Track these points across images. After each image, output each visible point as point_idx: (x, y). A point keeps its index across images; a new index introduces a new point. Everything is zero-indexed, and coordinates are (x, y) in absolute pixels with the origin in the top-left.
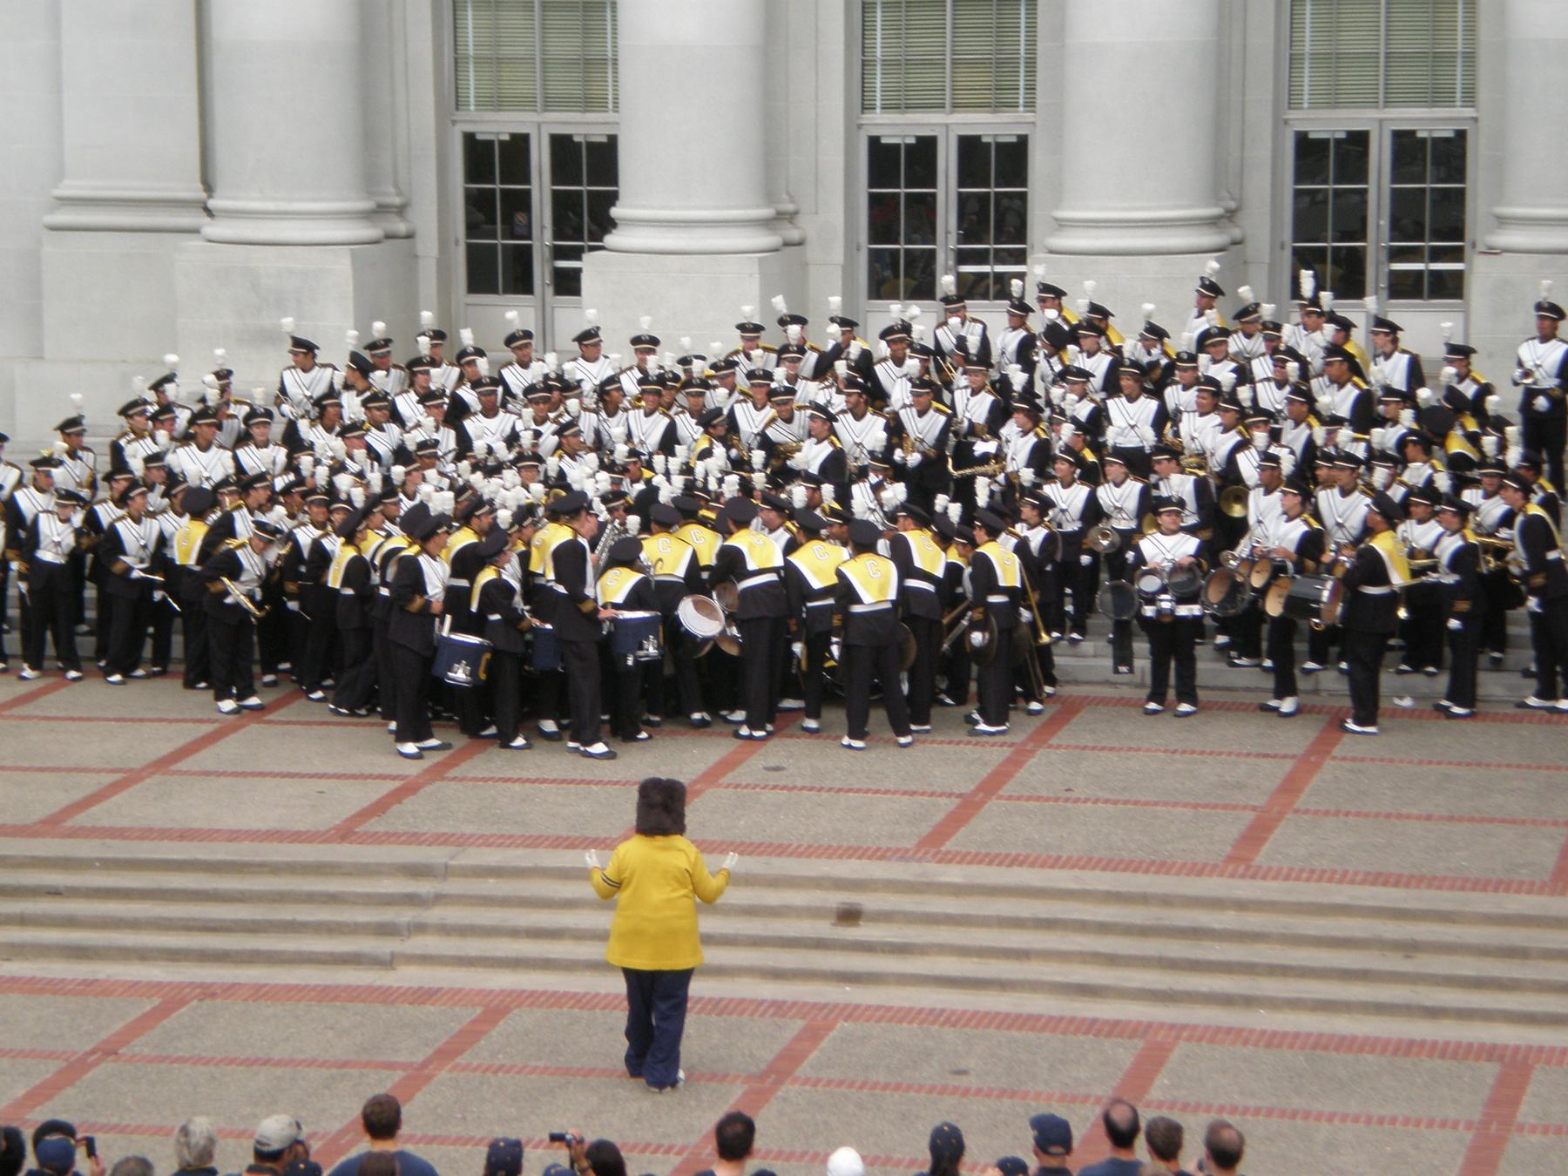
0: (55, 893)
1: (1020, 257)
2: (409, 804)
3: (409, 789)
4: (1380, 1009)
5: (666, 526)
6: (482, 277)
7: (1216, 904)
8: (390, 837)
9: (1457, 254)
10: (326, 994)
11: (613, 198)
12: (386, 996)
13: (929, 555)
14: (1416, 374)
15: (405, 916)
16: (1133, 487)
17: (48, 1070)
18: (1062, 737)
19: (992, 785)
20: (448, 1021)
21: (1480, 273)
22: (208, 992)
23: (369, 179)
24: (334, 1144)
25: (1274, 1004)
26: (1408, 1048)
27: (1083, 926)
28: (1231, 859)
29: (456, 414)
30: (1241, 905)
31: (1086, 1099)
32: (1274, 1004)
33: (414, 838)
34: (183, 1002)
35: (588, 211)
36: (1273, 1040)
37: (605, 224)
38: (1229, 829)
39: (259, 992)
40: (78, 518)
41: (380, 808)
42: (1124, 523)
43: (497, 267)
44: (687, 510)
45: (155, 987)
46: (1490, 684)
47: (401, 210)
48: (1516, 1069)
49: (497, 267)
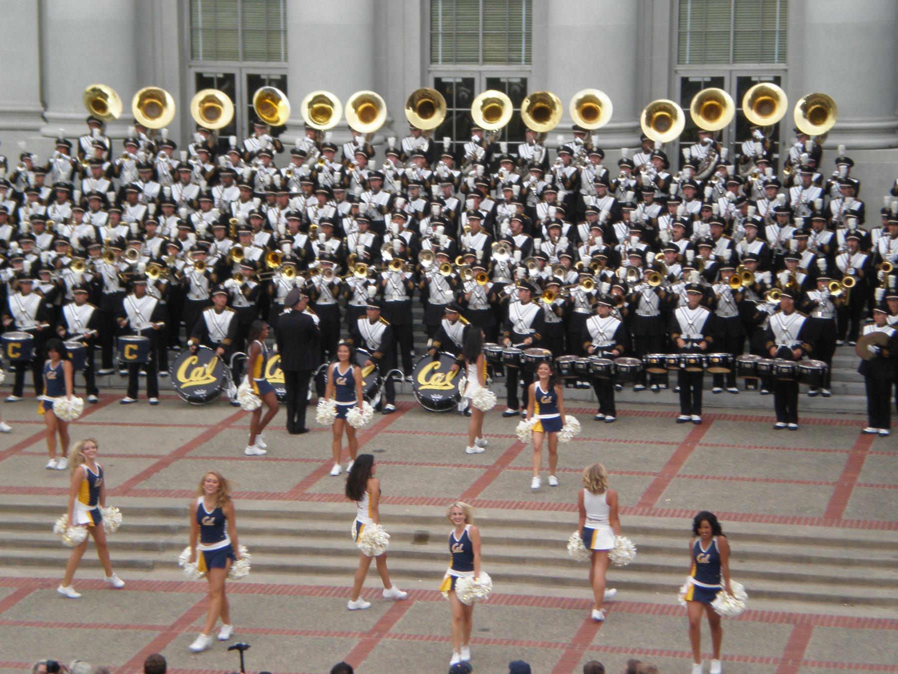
2: (164, 473)
8: (154, 493)
12: (150, 586)
28: (640, 504)
31: (556, 645)
33: (166, 493)
34: (31, 590)
48: (803, 628)
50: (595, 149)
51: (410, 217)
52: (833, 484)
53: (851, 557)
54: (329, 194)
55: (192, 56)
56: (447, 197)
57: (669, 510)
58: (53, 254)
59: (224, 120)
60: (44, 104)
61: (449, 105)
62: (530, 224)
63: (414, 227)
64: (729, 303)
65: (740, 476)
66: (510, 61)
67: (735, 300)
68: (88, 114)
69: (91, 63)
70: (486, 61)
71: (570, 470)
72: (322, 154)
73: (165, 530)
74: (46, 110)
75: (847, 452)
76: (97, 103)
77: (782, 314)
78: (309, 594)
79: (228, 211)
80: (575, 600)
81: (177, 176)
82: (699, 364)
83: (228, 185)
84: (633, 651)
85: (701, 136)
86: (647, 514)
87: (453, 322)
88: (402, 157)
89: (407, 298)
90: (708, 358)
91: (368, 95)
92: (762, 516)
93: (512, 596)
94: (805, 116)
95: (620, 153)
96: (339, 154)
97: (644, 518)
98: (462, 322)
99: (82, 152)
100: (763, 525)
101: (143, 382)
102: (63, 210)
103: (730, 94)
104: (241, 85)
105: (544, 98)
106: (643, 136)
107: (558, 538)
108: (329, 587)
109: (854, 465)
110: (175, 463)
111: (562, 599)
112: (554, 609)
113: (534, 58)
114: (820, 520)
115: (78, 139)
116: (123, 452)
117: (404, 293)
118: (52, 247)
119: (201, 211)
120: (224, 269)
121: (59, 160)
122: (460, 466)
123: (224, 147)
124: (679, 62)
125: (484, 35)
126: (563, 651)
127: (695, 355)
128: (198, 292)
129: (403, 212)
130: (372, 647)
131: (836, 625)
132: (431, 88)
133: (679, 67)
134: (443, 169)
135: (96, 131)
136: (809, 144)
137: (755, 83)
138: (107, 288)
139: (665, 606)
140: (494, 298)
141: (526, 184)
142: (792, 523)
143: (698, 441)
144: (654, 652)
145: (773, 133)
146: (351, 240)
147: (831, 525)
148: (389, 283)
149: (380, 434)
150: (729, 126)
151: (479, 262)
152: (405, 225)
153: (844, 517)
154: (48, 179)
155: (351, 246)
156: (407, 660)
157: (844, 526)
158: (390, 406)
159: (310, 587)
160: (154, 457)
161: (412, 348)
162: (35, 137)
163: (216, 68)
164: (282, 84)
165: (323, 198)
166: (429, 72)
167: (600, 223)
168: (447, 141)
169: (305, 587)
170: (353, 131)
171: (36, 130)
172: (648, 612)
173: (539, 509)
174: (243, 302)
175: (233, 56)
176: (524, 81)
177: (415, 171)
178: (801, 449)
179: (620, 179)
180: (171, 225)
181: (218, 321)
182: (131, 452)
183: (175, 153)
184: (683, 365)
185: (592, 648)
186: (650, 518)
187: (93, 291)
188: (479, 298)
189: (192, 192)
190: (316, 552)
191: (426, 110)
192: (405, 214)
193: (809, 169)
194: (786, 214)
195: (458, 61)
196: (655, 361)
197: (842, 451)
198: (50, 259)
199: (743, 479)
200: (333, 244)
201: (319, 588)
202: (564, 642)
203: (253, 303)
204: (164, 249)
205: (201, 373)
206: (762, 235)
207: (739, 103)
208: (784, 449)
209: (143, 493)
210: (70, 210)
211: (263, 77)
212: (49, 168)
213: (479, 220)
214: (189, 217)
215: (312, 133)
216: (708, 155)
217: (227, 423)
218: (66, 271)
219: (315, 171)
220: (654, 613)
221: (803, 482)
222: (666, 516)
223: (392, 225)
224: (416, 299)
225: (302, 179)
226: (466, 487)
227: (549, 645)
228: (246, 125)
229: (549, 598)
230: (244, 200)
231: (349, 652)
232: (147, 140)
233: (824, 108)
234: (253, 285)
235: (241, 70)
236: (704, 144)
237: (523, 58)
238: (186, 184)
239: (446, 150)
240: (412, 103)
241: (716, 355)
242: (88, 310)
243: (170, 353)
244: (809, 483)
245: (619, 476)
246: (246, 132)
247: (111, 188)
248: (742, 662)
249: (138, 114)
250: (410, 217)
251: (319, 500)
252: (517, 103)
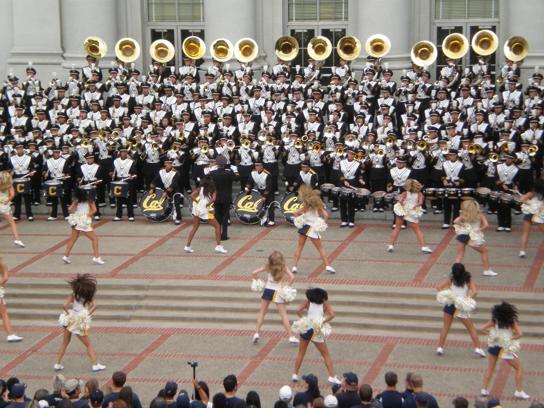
2: (135, 264)
8: (129, 276)
12: (128, 331)
15: (135, 303)
27: (364, 304)
28: (414, 280)
31: (365, 364)
33: (137, 276)
50: (387, 71)
51: (276, 113)
52: (529, 267)
53: (539, 310)
54: (230, 100)
55: (289, 20)
56: (298, 100)
57: (431, 284)
58: (71, 136)
59: (169, 58)
60: (63, 49)
61: (300, 46)
62: (350, 116)
63: (278, 119)
64: (467, 161)
65: (474, 263)
66: (336, 19)
67: (471, 159)
68: (86, 55)
69: (90, 23)
70: (180, 20)
71: (373, 261)
72: (223, 76)
73: (137, 298)
74: (64, 53)
75: (537, 248)
76: (93, 47)
77: (504, 164)
78: (221, 334)
79: (170, 111)
80: (376, 337)
81: (140, 90)
82: (456, 194)
83: (169, 96)
84: (411, 367)
85: (448, 62)
86: (419, 286)
87: (306, 173)
88: (273, 77)
89: (276, 161)
90: (461, 191)
91: (247, 41)
92: (487, 286)
93: (339, 335)
94: (510, 50)
95: (402, 72)
96: (234, 77)
97: (417, 288)
98: (311, 172)
99: (85, 77)
100: (487, 292)
101: (125, 211)
102: (76, 112)
103: (466, 37)
104: (177, 36)
105: (351, 40)
106: (412, 62)
107: (365, 301)
108: (231, 331)
110: (142, 259)
111: (369, 336)
112: (364, 343)
113: (349, 17)
114: (521, 288)
115: (82, 69)
116: (112, 252)
117: (274, 158)
118: (69, 132)
119: (155, 111)
120: (168, 145)
121: (72, 83)
122: (307, 259)
123: (166, 73)
124: (289, 20)
125: (320, 4)
126: (370, 367)
127: (454, 189)
128: (153, 158)
129: (271, 110)
130: (258, 365)
131: (531, 350)
132: (289, 35)
133: (436, 21)
134: (296, 84)
135: (93, 65)
136: (514, 67)
137: (481, 29)
138: (102, 156)
139: (429, 340)
140: (325, 159)
141: (346, 92)
142: (505, 290)
143: (448, 243)
144: (423, 367)
145: (492, 60)
146: (241, 127)
147: (527, 291)
148: (265, 151)
149: (260, 241)
150: (466, 55)
151: (317, 139)
152: (273, 117)
153: (535, 286)
154: (67, 94)
155: (241, 130)
156: (278, 373)
157: (535, 292)
158: (271, 223)
159: (221, 330)
160: (131, 255)
161: (277, 190)
162: (58, 68)
163: (162, 27)
164: (201, 34)
165: (226, 102)
166: (288, 26)
167: (293, 131)
168: (298, 67)
169: (218, 330)
170: (240, 62)
171: (60, 64)
172: (419, 343)
173: (354, 284)
174: (177, 163)
175: (173, 19)
176: (344, 31)
177: (278, 85)
178: (510, 247)
179: (401, 88)
180: (137, 120)
181: (167, 176)
182: (116, 253)
183: (139, 77)
184: (446, 195)
185: (387, 365)
186: (420, 288)
187: (94, 157)
188: (316, 159)
189: (150, 99)
190: (224, 310)
191: (287, 49)
192: (273, 112)
193: (514, 81)
194: (501, 106)
195: (304, 19)
196: (430, 193)
197: (534, 247)
198: (69, 140)
199: (475, 265)
200: (232, 129)
201: (226, 331)
202: (370, 361)
203: (182, 164)
204: (133, 133)
205: (155, 204)
206: (486, 120)
207: (471, 43)
208: (499, 246)
210: (79, 111)
211: (190, 31)
212: (66, 88)
213: (315, 115)
214: (148, 114)
215: (217, 64)
216: (452, 73)
217: (172, 235)
218: (78, 147)
219: (221, 86)
220: (423, 344)
221: (511, 266)
222: (430, 287)
223: (265, 118)
224: (280, 161)
225: (213, 91)
226: (311, 271)
227: (361, 364)
228: (181, 60)
229: (361, 336)
230: (178, 103)
231: (244, 368)
232: (123, 69)
233: (521, 44)
234: (182, 153)
235: (177, 27)
236: (450, 67)
237: (343, 17)
238: (146, 95)
239: (298, 73)
240: (278, 47)
241: (467, 189)
242: (95, 167)
243: (138, 194)
244: (514, 266)
245: (401, 264)
246: (181, 64)
247: (101, 98)
248: (475, 372)
249: (119, 54)
250: (276, 113)
251: (225, 280)
252: (334, 44)
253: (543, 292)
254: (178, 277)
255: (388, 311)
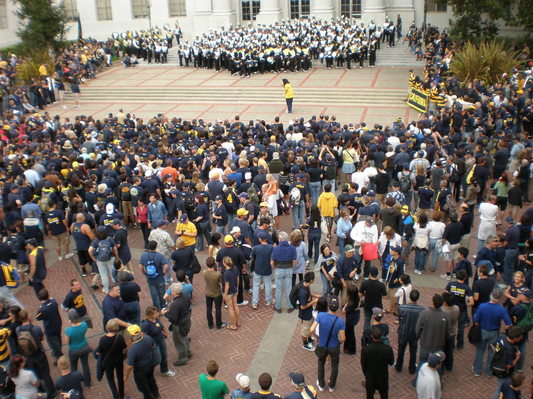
0: (199, 93)
1: (309, 14)
2: (238, 82)
3: (238, 81)
4: (351, 102)
5: (268, 48)
6: (244, 19)
7: (333, 91)
8: (236, 86)
9: (360, 13)
10: (230, 104)
11: (260, 8)
12: (237, 105)
13: (299, 50)
14: (357, 27)
15: (239, 95)
16: (325, 41)
17: (200, 113)
18: (315, 72)
19: (307, 78)
20: (244, 108)
21: (363, 15)
22: (217, 104)
23: (231, 7)
24: (232, 121)
25: (339, 102)
26: (355, 107)
27: (318, 94)
29: (242, 35)
30: (336, 91)
32: (339, 102)
33: (239, 86)
35: (257, 11)
36: (339, 106)
37: (259, 11)
38: (335, 82)
39: (223, 104)
40: (198, 49)
41: (235, 83)
42: (323, 46)
43: (246, 17)
44: (270, 46)
45: (211, 104)
46: (364, 64)
47: (235, 11)
48: (366, 109)
49: (246, 17)
109: (377, 76)
209: (235, 87)
253: (359, 2)
254: (253, 87)
255: (326, 96)
